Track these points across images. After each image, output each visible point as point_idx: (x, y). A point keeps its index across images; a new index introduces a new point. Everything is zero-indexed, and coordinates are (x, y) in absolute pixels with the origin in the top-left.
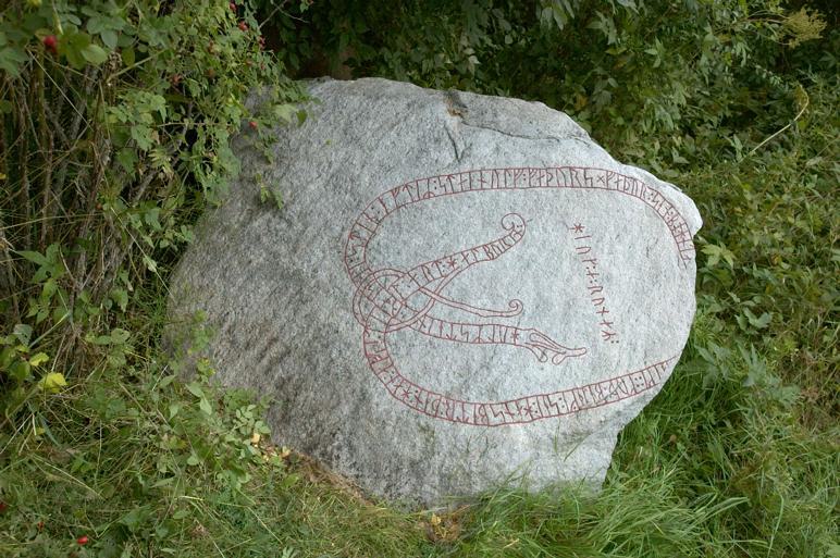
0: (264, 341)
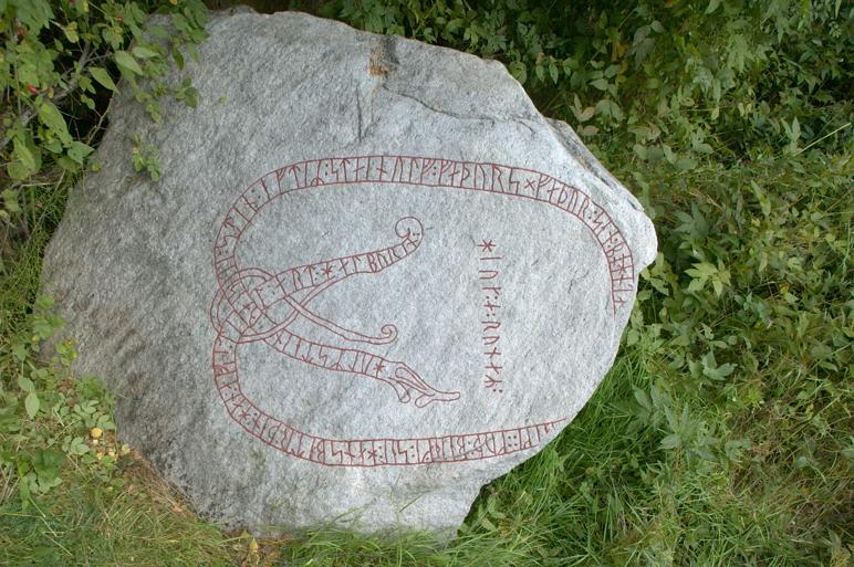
0: (122, 332)
